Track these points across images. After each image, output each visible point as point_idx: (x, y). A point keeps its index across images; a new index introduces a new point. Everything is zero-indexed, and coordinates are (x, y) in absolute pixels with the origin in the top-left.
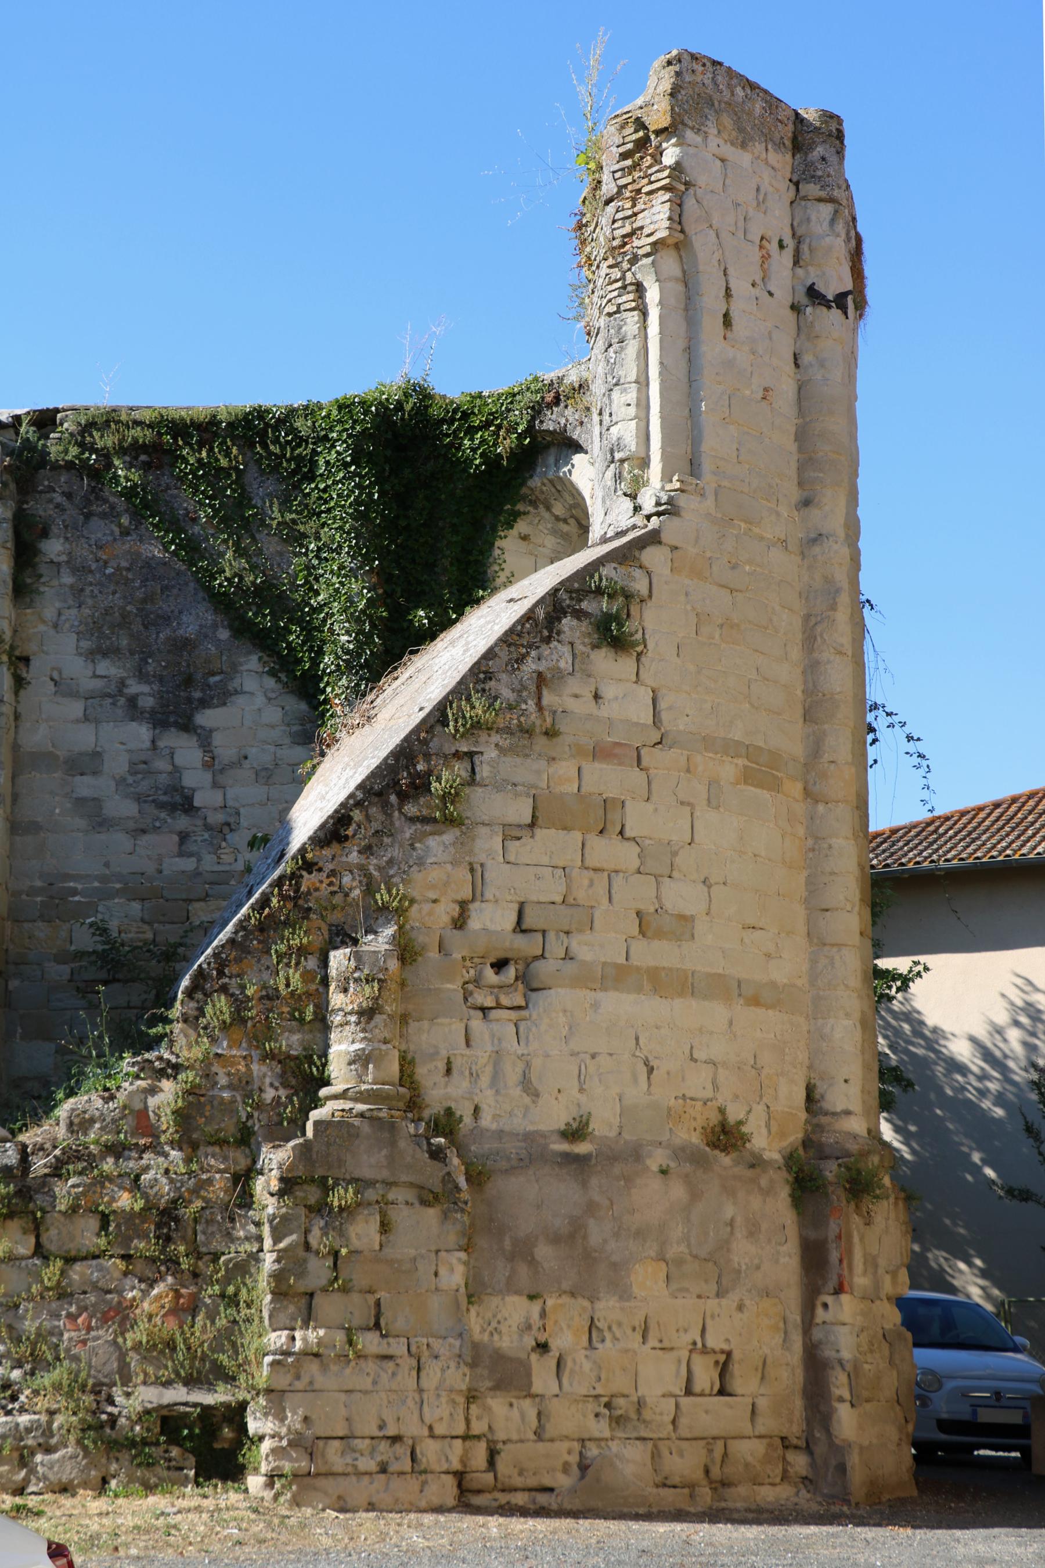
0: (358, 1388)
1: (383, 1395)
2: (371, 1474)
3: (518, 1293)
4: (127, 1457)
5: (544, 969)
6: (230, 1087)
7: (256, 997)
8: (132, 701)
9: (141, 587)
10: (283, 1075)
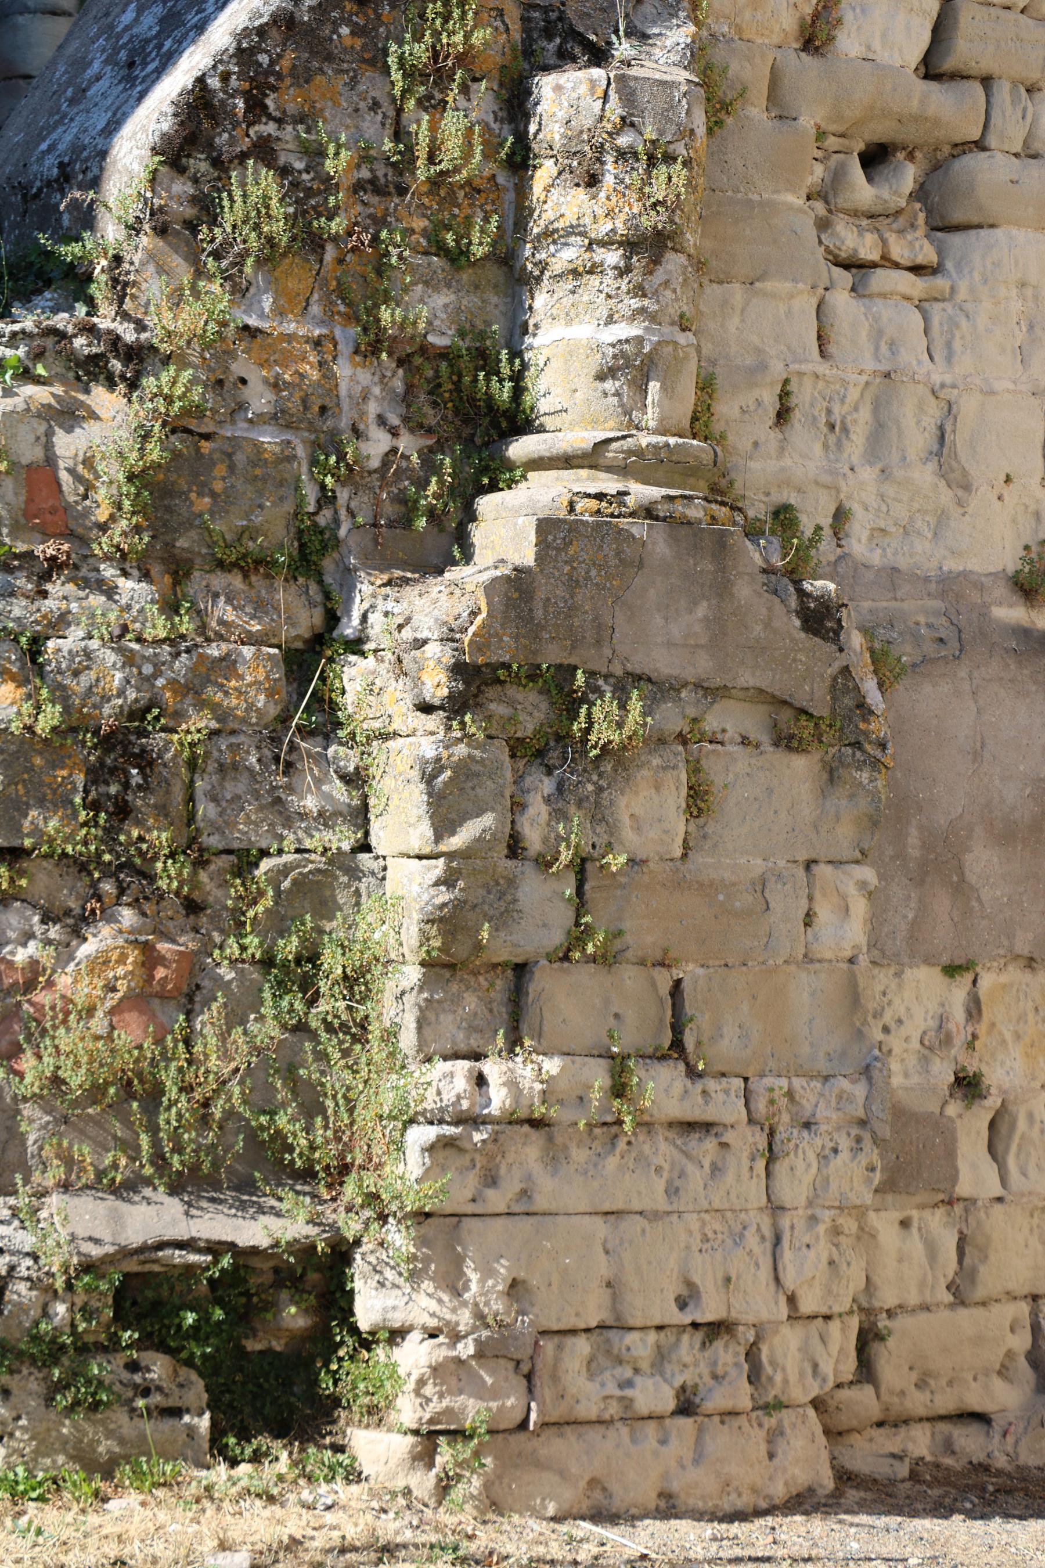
0: (636, 1206)
1: (692, 1221)
2: (661, 1418)
3: (928, 961)
4: (33, 1385)
5: (990, 173)
6: (279, 418)
7: (347, 182)
10: (408, 397)
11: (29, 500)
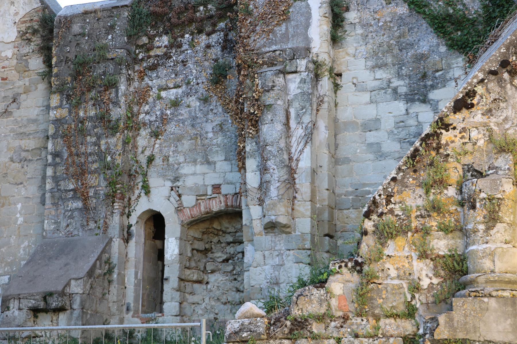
8: (395, 90)
9: (397, 30)
11: (339, 304)
